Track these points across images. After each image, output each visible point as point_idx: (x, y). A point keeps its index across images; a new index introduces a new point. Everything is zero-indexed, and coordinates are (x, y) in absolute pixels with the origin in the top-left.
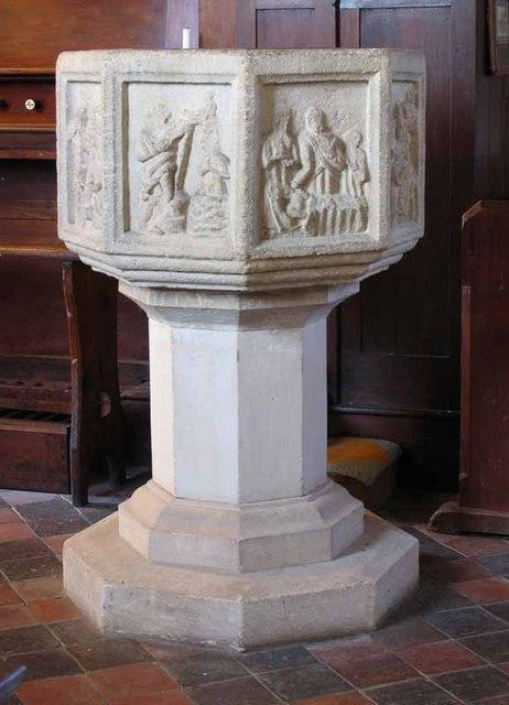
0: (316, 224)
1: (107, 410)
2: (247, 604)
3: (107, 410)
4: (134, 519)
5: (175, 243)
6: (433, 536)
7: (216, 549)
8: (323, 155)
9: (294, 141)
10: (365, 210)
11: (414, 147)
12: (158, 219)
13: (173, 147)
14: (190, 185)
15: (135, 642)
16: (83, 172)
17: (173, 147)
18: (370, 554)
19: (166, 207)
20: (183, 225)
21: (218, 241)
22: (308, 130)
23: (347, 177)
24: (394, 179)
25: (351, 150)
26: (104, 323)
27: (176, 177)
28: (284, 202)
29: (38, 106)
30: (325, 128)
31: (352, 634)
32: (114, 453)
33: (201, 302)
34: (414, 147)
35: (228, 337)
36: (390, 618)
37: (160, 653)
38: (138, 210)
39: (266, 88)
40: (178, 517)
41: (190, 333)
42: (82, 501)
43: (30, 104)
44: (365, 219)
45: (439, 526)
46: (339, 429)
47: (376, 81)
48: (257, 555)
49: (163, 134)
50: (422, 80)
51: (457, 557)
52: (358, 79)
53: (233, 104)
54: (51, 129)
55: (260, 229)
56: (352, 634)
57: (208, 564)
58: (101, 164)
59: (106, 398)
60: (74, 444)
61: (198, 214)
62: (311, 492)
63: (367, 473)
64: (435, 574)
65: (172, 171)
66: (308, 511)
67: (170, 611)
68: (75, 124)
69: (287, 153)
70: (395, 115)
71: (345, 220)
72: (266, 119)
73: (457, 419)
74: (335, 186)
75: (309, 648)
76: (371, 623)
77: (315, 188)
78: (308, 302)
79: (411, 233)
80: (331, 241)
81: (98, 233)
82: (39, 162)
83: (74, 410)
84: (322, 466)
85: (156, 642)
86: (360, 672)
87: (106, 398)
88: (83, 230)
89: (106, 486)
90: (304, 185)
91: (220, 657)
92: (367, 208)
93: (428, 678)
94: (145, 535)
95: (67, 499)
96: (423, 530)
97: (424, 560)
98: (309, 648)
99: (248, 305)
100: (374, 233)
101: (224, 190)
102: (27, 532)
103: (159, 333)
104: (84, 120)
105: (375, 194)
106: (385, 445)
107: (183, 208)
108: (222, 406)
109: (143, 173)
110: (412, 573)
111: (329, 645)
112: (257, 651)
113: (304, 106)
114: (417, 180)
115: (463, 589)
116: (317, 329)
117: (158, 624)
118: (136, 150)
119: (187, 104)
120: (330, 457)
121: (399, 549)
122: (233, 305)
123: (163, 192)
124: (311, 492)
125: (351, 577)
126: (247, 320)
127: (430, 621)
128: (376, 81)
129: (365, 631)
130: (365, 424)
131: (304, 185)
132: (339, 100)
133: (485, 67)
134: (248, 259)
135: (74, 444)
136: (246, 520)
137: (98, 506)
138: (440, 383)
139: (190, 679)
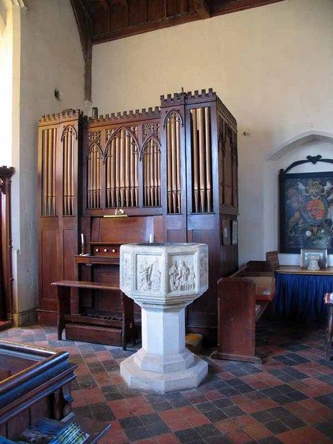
0: (182, 288)
1: (131, 327)
2: (166, 383)
3: (131, 327)
4: (137, 358)
5: (148, 293)
6: (212, 360)
7: (158, 367)
8: (184, 271)
9: (177, 268)
10: (194, 284)
11: (206, 268)
12: (144, 287)
13: (148, 270)
14: (152, 279)
15: (137, 390)
16: (126, 274)
17: (148, 270)
18: (196, 367)
19: (146, 284)
20: (150, 289)
21: (159, 293)
22: (180, 266)
23: (190, 277)
24: (201, 276)
25: (191, 270)
26: (131, 310)
27: (148, 277)
28: (174, 283)
29: (116, 251)
30: (184, 265)
31: (192, 389)
32: (133, 338)
33: (154, 306)
34: (206, 268)
35: (161, 314)
36: (201, 384)
37: (144, 394)
38: (139, 284)
39: (170, 256)
40: (147, 359)
41: (152, 313)
42: (125, 349)
43: (114, 251)
44: (194, 287)
45: (213, 357)
46: (188, 331)
47: (196, 254)
48: (168, 368)
49: (145, 267)
50: (207, 251)
51: (217, 366)
52: (192, 253)
53: (162, 260)
54: (116, 263)
55: (169, 290)
56: (192, 389)
57: (156, 370)
58: (130, 273)
59: (131, 324)
60: (123, 335)
61: (153, 287)
62: (181, 352)
63: (195, 343)
64: (212, 370)
65: (147, 276)
66: (181, 357)
67: (146, 383)
68: (124, 263)
69: (175, 271)
70: (201, 260)
71: (189, 287)
72: (170, 264)
73: (216, 330)
74: (187, 278)
75: (181, 392)
76: (196, 386)
77: (182, 279)
78: (181, 306)
79: (205, 288)
80: (185, 293)
81: (130, 290)
82: (116, 265)
83: (123, 326)
84: (184, 342)
85: (143, 391)
86: (194, 400)
87: (131, 324)
88: (126, 288)
89: (131, 345)
90: (179, 279)
91: (158, 395)
92: (195, 283)
93: (210, 401)
94: (140, 362)
95: (121, 348)
96: (209, 358)
97: (209, 367)
98: (181, 392)
99: (166, 307)
100: (196, 290)
101: (160, 281)
102: (111, 358)
103: (144, 312)
104: (126, 262)
105: (197, 281)
106: (200, 335)
107: (150, 284)
108: (160, 331)
109: (141, 275)
110: (206, 372)
111: (187, 391)
112: (168, 394)
113: (179, 260)
114: (206, 275)
115: (219, 375)
116: (183, 312)
117: (143, 386)
118: (139, 270)
119: (151, 260)
120: (186, 339)
121: (203, 366)
122: (162, 307)
123: (145, 281)
124: (181, 352)
125: (190, 374)
126: (165, 311)
127: (211, 384)
128: (196, 254)
129: (195, 388)
130: (195, 330)
131: (179, 279)
132: (187, 259)
133: (222, 243)
134: (166, 297)
135: (123, 335)
136: (166, 360)
137: (130, 351)
138: (213, 320)
139: (152, 401)
